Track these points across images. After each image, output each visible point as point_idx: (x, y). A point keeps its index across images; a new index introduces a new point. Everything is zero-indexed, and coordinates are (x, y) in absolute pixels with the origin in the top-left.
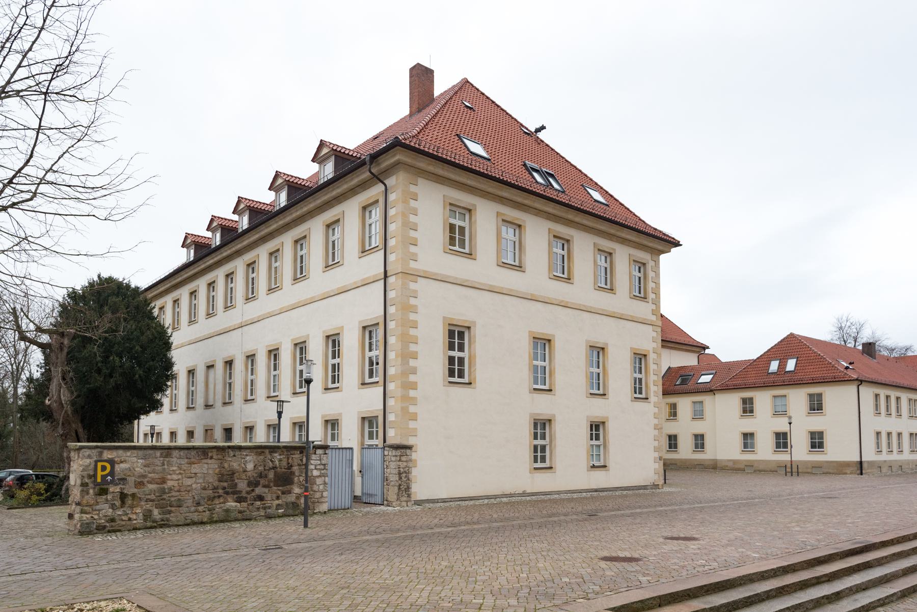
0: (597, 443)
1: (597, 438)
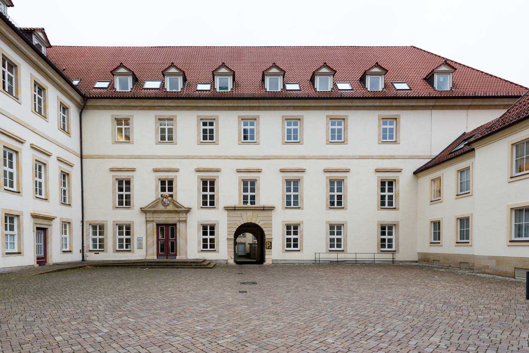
0: (12, 233)
1: (12, 228)
